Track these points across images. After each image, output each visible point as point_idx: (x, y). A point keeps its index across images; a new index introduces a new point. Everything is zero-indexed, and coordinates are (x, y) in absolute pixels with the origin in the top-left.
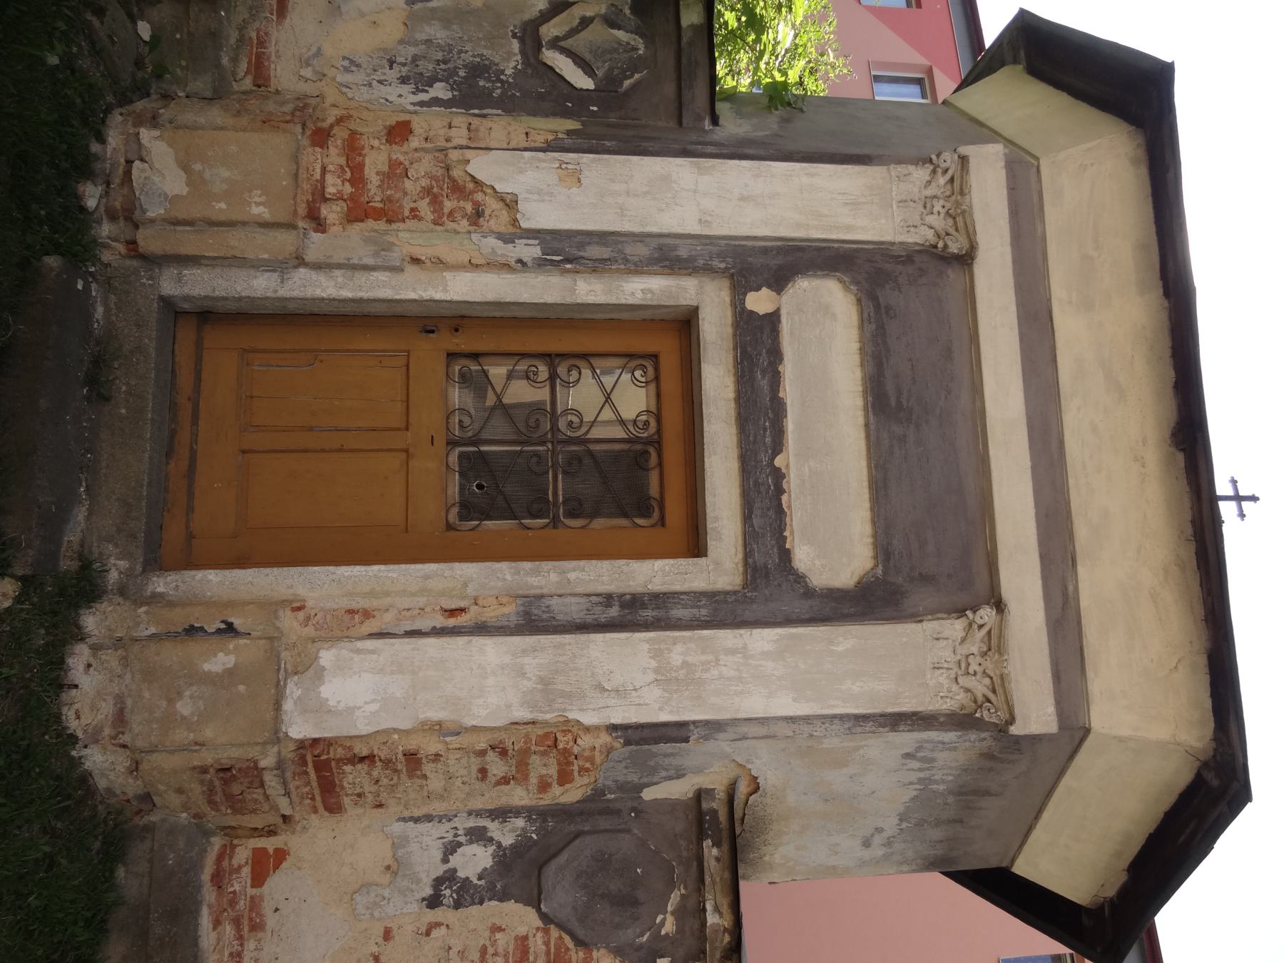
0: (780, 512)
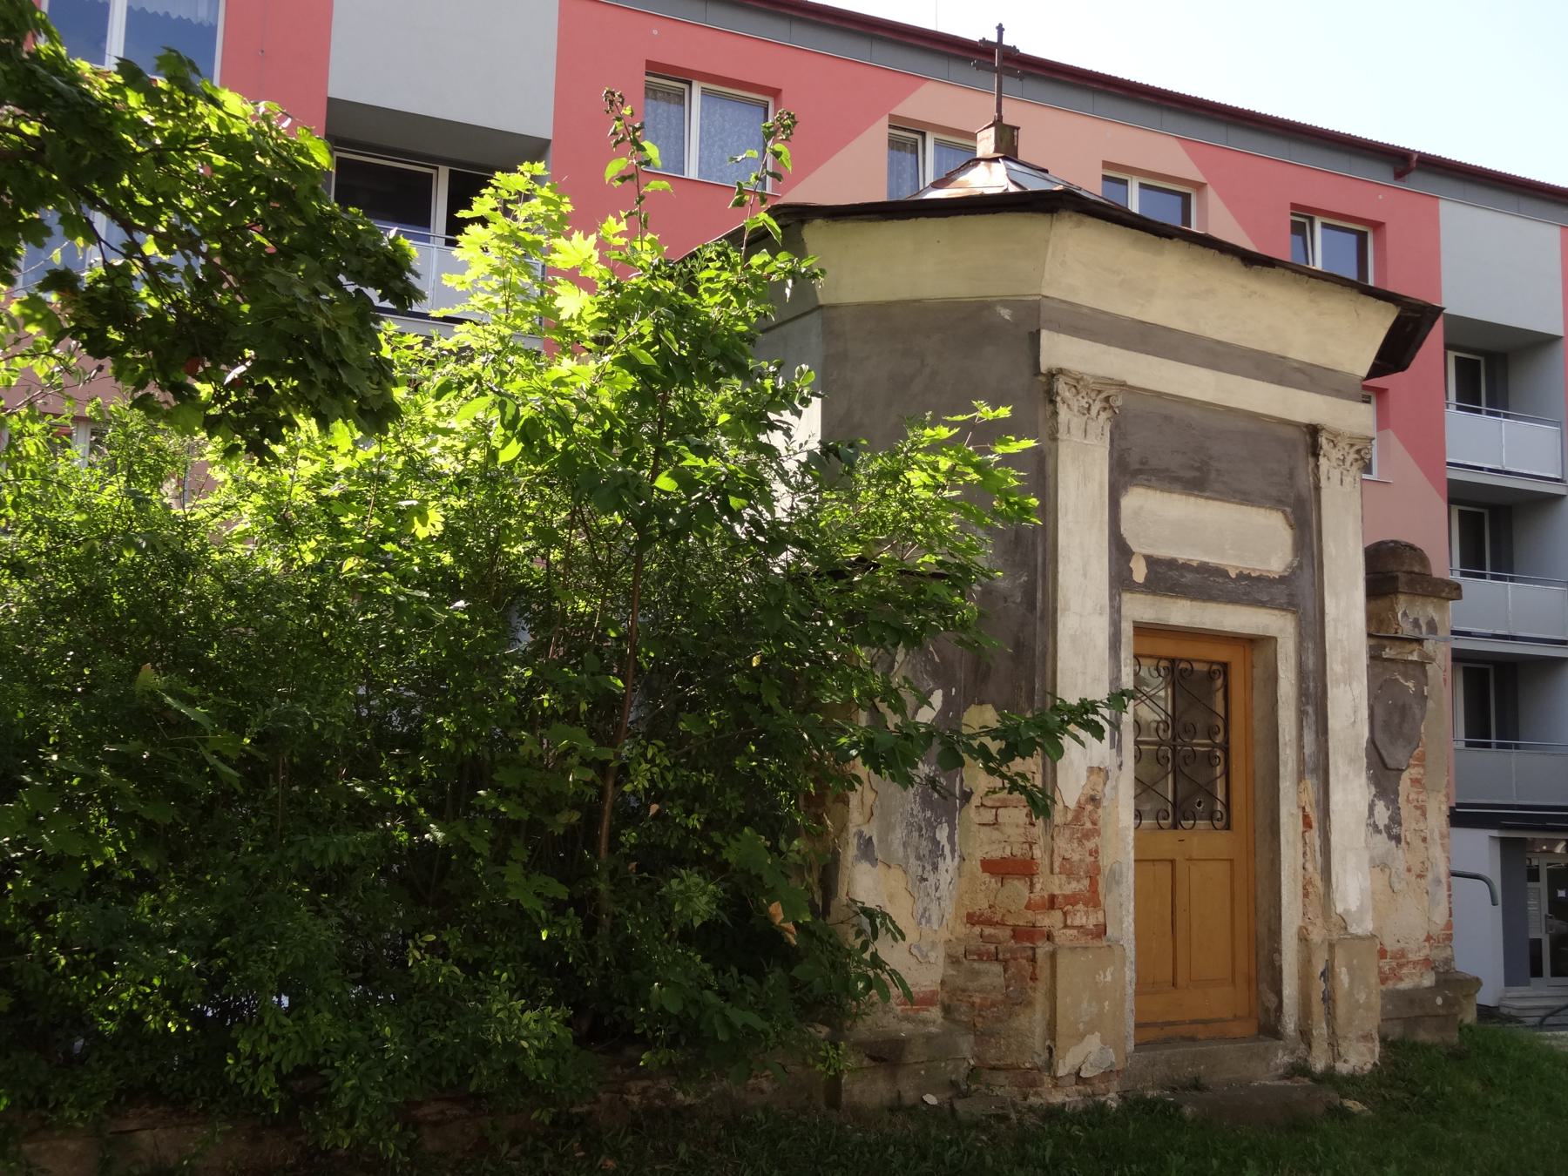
0: (1260, 579)
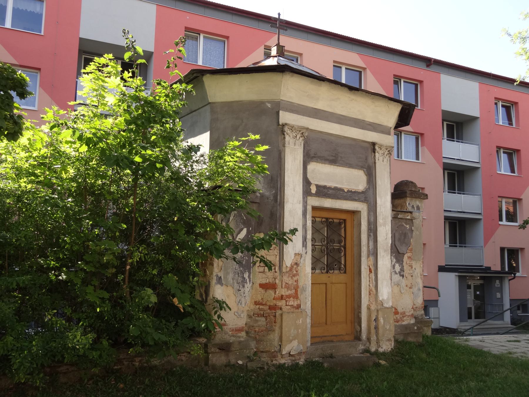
0: (355, 192)
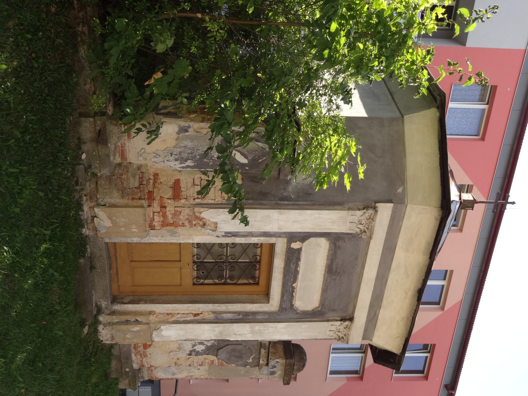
0: (292, 296)
